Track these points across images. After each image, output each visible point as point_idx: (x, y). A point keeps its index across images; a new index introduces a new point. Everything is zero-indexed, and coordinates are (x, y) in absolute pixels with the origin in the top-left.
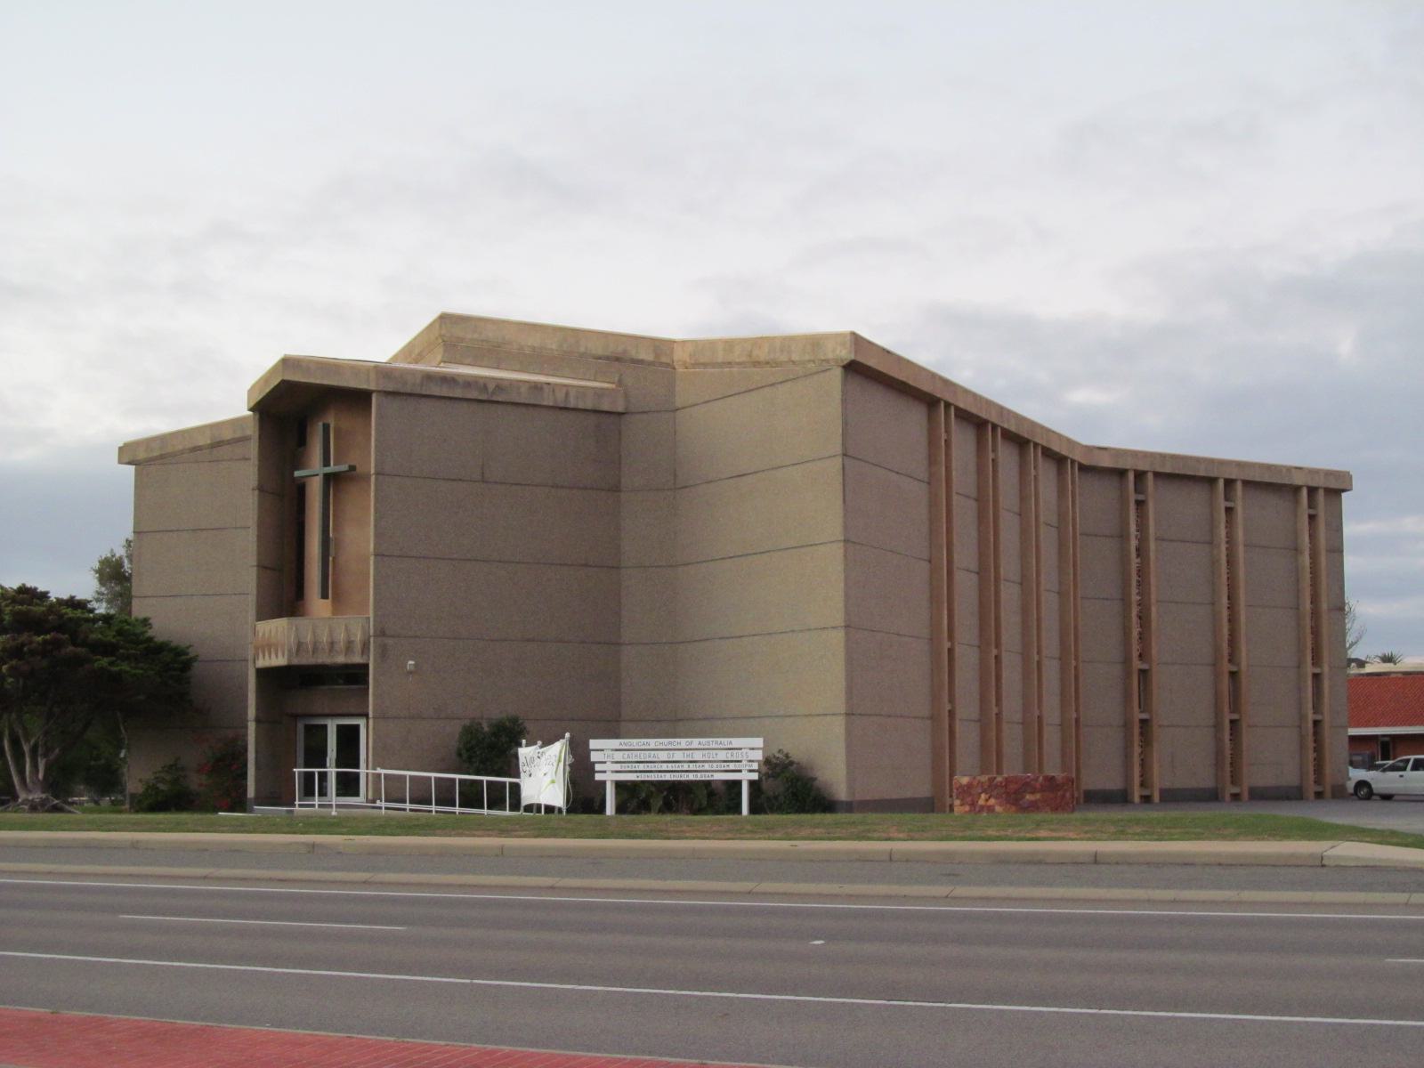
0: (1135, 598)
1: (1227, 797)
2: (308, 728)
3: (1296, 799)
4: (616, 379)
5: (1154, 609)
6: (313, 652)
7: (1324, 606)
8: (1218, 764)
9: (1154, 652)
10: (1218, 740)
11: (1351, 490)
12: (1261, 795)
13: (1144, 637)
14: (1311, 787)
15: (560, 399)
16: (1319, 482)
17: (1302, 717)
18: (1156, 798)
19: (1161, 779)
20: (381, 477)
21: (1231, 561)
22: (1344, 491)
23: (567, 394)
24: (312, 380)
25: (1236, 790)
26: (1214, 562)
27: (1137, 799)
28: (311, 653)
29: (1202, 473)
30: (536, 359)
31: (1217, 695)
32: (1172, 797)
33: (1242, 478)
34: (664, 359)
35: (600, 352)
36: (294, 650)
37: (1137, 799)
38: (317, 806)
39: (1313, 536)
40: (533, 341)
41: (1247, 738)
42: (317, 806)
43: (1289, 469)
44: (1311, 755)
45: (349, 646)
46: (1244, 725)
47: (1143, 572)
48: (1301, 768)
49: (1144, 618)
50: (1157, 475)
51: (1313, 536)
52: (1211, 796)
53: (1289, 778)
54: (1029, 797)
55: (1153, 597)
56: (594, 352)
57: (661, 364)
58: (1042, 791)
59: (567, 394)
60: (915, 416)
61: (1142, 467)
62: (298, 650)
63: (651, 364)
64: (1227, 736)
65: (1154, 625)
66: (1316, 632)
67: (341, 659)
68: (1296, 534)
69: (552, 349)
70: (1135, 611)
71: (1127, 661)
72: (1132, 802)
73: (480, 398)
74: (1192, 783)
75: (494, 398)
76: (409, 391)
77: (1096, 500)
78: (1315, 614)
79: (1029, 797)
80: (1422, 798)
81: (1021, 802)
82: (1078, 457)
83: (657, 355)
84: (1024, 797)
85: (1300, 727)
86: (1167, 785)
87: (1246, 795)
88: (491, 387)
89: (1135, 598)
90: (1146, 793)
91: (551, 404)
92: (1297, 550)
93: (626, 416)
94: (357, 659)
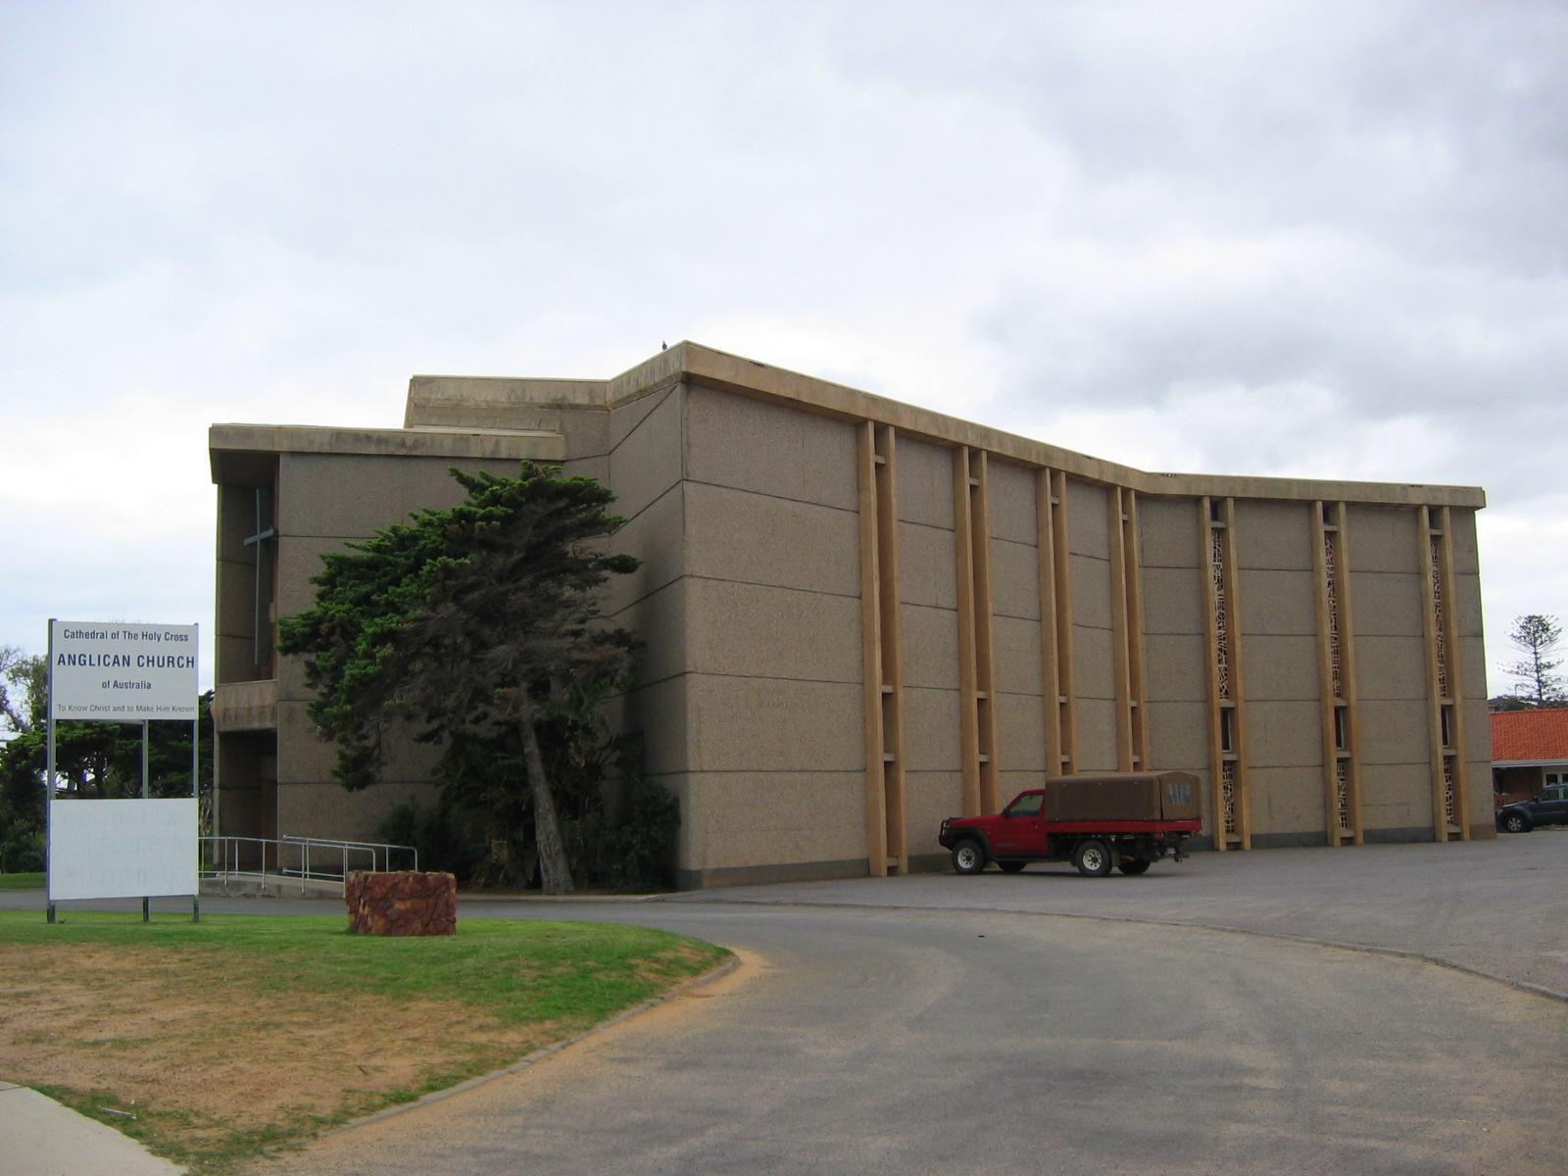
0: (1214, 630)
1: (1337, 841)
2: (1228, 749)
3: (1427, 841)
4: (557, 427)
5: (1238, 643)
6: (236, 719)
7: (1454, 633)
8: (1326, 805)
9: (1240, 687)
10: (1326, 781)
11: (1485, 506)
12: (1378, 838)
13: (1228, 673)
14: (1445, 828)
15: (488, 450)
16: (1446, 500)
17: (1432, 753)
18: (1360, 839)
19: (1369, 818)
20: (1353, 574)
21: (1335, 586)
22: (1479, 508)
23: (497, 442)
24: (231, 447)
25: (1348, 834)
26: (1315, 592)
27: (1222, 846)
28: (233, 719)
29: (1295, 496)
30: (490, 413)
31: (1323, 731)
32: (1268, 843)
33: (1346, 499)
34: (599, 402)
35: (543, 400)
36: (221, 717)
37: (1222, 846)
38: (1560, 779)
39: (1438, 559)
40: (485, 396)
41: (1360, 775)
42: (1560, 779)
43: (1404, 488)
44: (1443, 791)
45: (262, 714)
46: (1356, 762)
47: (1225, 605)
48: (1433, 808)
49: (1227, 652)
50: (1238, 500)
51: (1438, 559)
52: (1320, 840)
53: (1419, 819)
54: (399, 906)
55: (1237, 633)
56: (537, 401)
57: (597, 407)
58: (412, 895)
59: (497, 442)
60: (831, 449)
61: (1218, 492)
62: (224, 717)
63: (587, 408)
64: (1335, 779)
65: (1238, 659)
66: (1446, 660)
67: (256, 725)
68: (1419, 556)
69: (502, 402)
70: (1215, 646)
71: (1207, 700)
72: (1218, 850)
73: (396, 453)
74: (1408, 823)
75: (414, 453)
76: (316, 450)
77: (1169, 534)
78: (1445, 642)
79: (399, 906)
80: (2, 1001)
81: (389, 912)
82: (1134, 484)
83: (592, 399)
84: (392, 906)
85: (1430, 763)
86: (1259, 830)
87: (1360, 839)
88: (409, 442)
89: (1214, 630)
90: (1235, 839)
91: (481, 456)
92: (1420, 574)
93: (567, 463)
94: (268, 725)
